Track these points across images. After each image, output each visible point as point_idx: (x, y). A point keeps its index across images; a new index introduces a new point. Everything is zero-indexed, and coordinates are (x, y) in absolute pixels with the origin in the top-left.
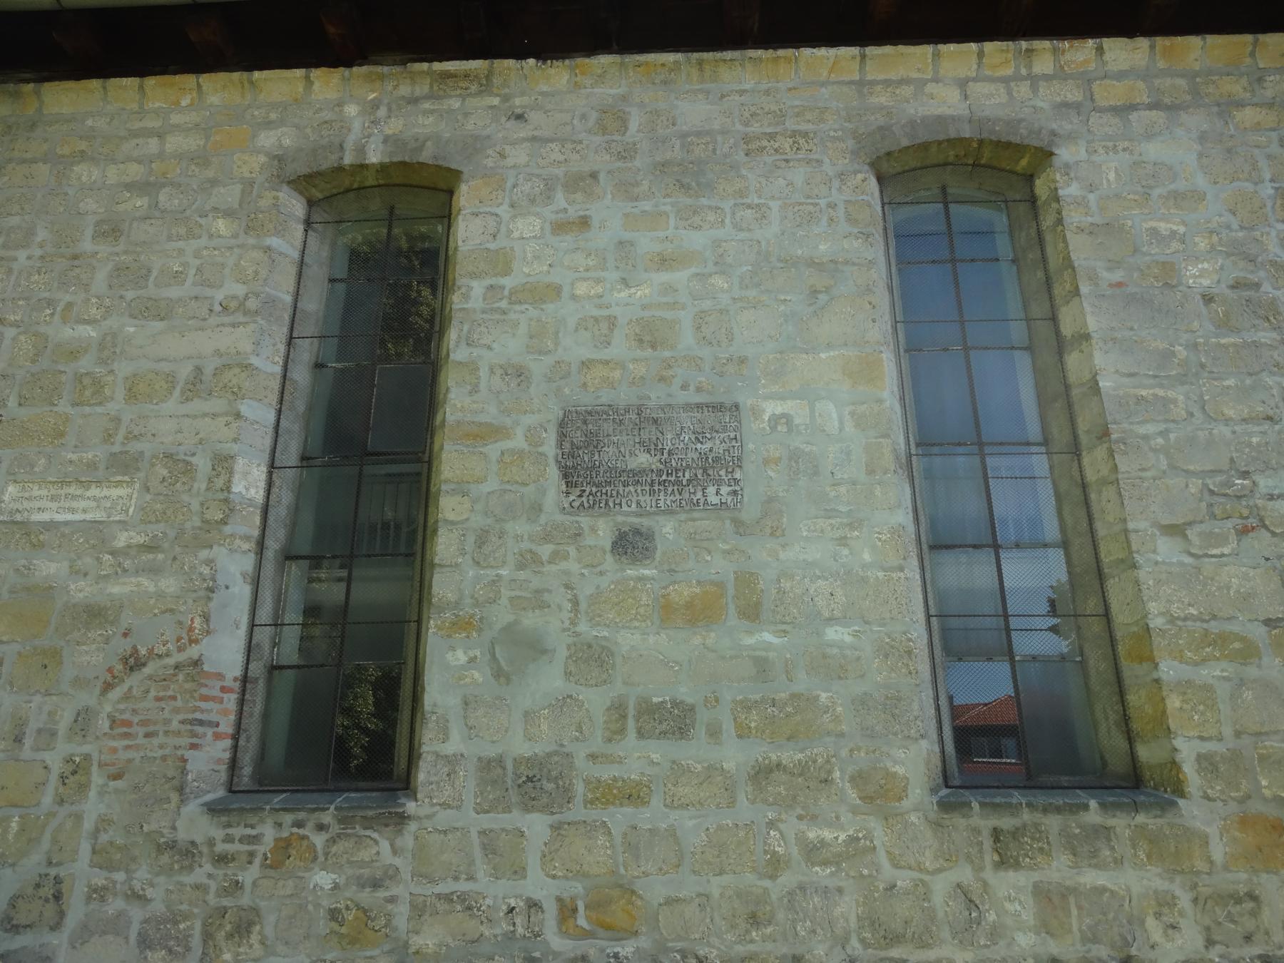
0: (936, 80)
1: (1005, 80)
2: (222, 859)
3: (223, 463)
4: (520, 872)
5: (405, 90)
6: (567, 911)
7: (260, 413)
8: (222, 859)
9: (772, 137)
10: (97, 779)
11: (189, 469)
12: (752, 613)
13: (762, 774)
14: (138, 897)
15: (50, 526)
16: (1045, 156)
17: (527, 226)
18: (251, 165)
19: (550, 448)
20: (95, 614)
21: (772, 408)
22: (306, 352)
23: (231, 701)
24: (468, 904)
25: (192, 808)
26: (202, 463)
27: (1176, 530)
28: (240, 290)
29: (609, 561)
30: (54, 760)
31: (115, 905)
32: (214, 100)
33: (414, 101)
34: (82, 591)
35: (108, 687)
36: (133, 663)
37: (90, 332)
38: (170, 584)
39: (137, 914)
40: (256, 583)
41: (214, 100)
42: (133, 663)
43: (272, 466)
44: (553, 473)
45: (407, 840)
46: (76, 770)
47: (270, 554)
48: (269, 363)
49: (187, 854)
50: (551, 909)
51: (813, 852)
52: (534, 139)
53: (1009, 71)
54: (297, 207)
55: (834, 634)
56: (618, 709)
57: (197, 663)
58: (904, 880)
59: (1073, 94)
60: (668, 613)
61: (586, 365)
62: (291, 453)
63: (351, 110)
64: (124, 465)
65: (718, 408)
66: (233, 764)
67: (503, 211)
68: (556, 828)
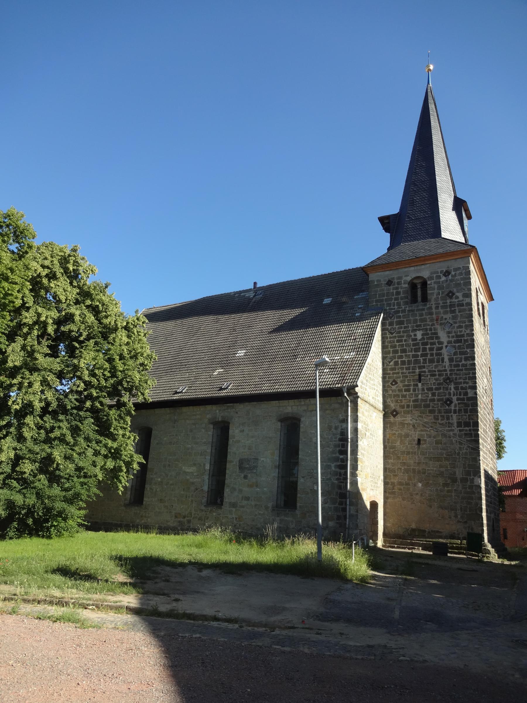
0: (288, 406)
1: (297, 406)
2: (205, 511)
3: (204, 465)
4: (232, 514)
5: (223, 408)
6: (236, 519)
7: (208, 458)
8: (205, 511)
9: (266, 416)
10: (194, 502)
11: (201, 465)
12: (257, 486)
13: (256, 505)
14: (198, 515)
15: (188, 472)
16: (299, 420)
17: (237, 431)
18: (206, 421)
19: (238, 464)
20: (193, 483)
21: (262, 459)
22: (214, 448)
23: (207, 493)
24: (227, 517)
25: (203, 506)
26: (202, 465)
27: (303, 477)
28: (205, 440)
29: (243, 479)
30: (190, 500)
31: (196, 515)
32: (201, 409)
33: (224, 410)
34: (191, 480)
35: (195, 492)
36: (197, 489)
37: (190, 446)
38: (200, 480)
39: (198, 516)
40: (209, 479)
41: (201, 409)
42: (197, 489)
43: (210, 464)
44: (238, 467)
45: (222, 510)
46: (192, 501)
47: (210, 476)
48: (209, 451)
49: (202, 510)
50: (235, 518)
51: (259, 514)
52: (239, 417)
53: (298, 404)
54: (211, 426)
55: (265, 489)
56: (243, 497)
57: (203, 489)
58: (268, 518)
59: (305, 408)
60: (251, 486)
61: (243, 452)
62: (213, 463)
63: (217, 411)
64: (195, 465)
65: (256, 459)
66: (207, 501)
67: (234, 429)
68: (236, 510)
